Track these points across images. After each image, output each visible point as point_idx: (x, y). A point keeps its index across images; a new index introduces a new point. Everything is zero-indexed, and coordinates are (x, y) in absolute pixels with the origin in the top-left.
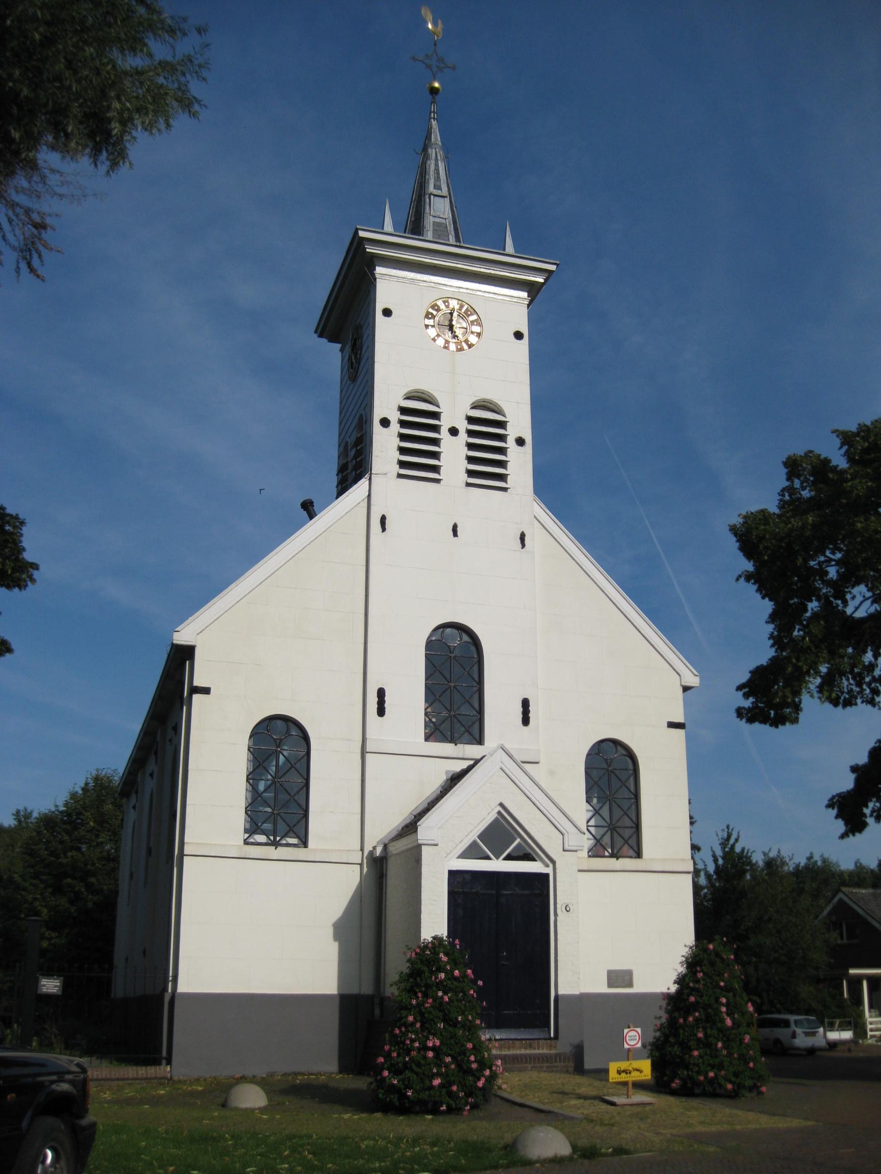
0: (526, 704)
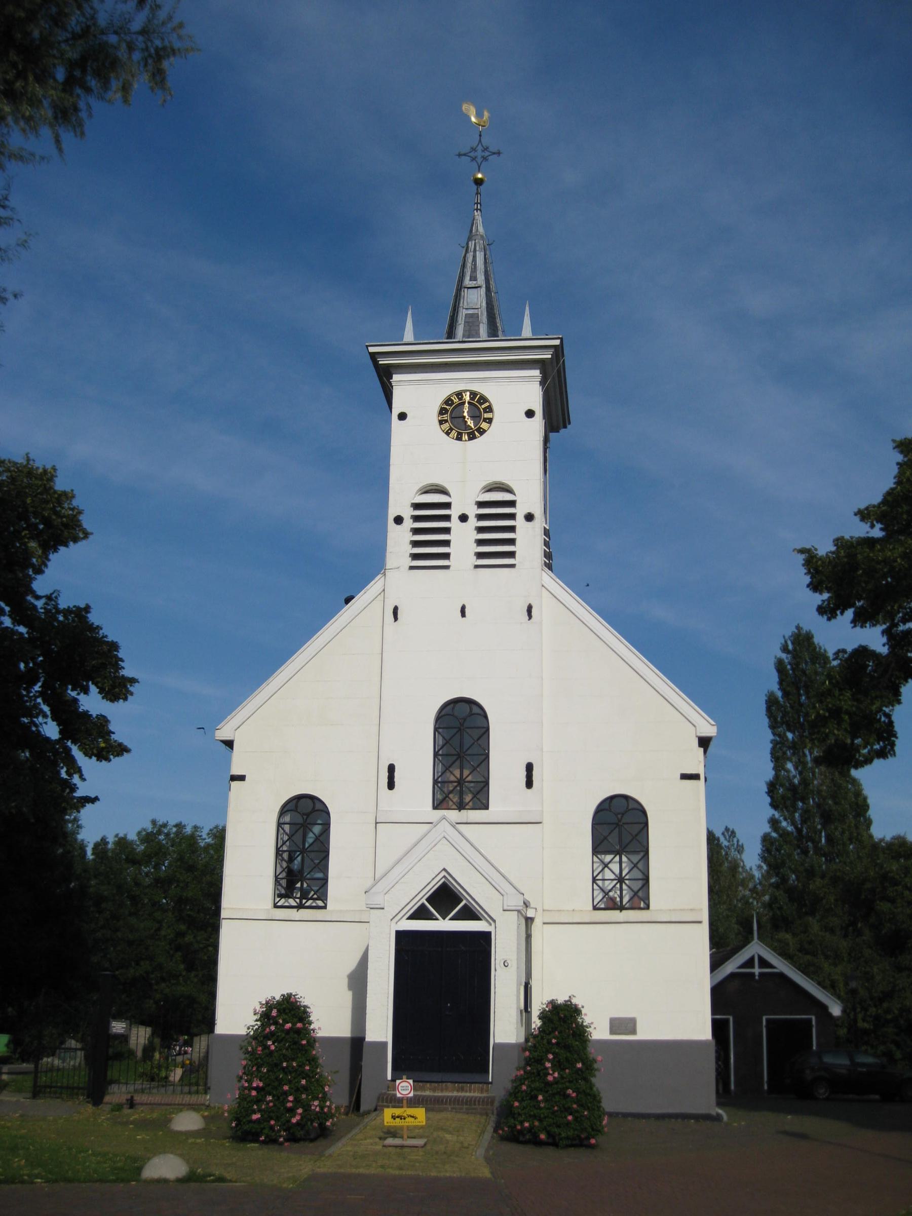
0: (529, 768)
